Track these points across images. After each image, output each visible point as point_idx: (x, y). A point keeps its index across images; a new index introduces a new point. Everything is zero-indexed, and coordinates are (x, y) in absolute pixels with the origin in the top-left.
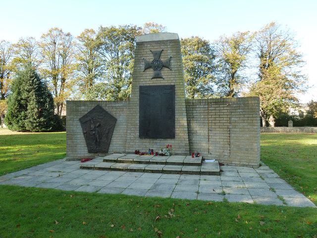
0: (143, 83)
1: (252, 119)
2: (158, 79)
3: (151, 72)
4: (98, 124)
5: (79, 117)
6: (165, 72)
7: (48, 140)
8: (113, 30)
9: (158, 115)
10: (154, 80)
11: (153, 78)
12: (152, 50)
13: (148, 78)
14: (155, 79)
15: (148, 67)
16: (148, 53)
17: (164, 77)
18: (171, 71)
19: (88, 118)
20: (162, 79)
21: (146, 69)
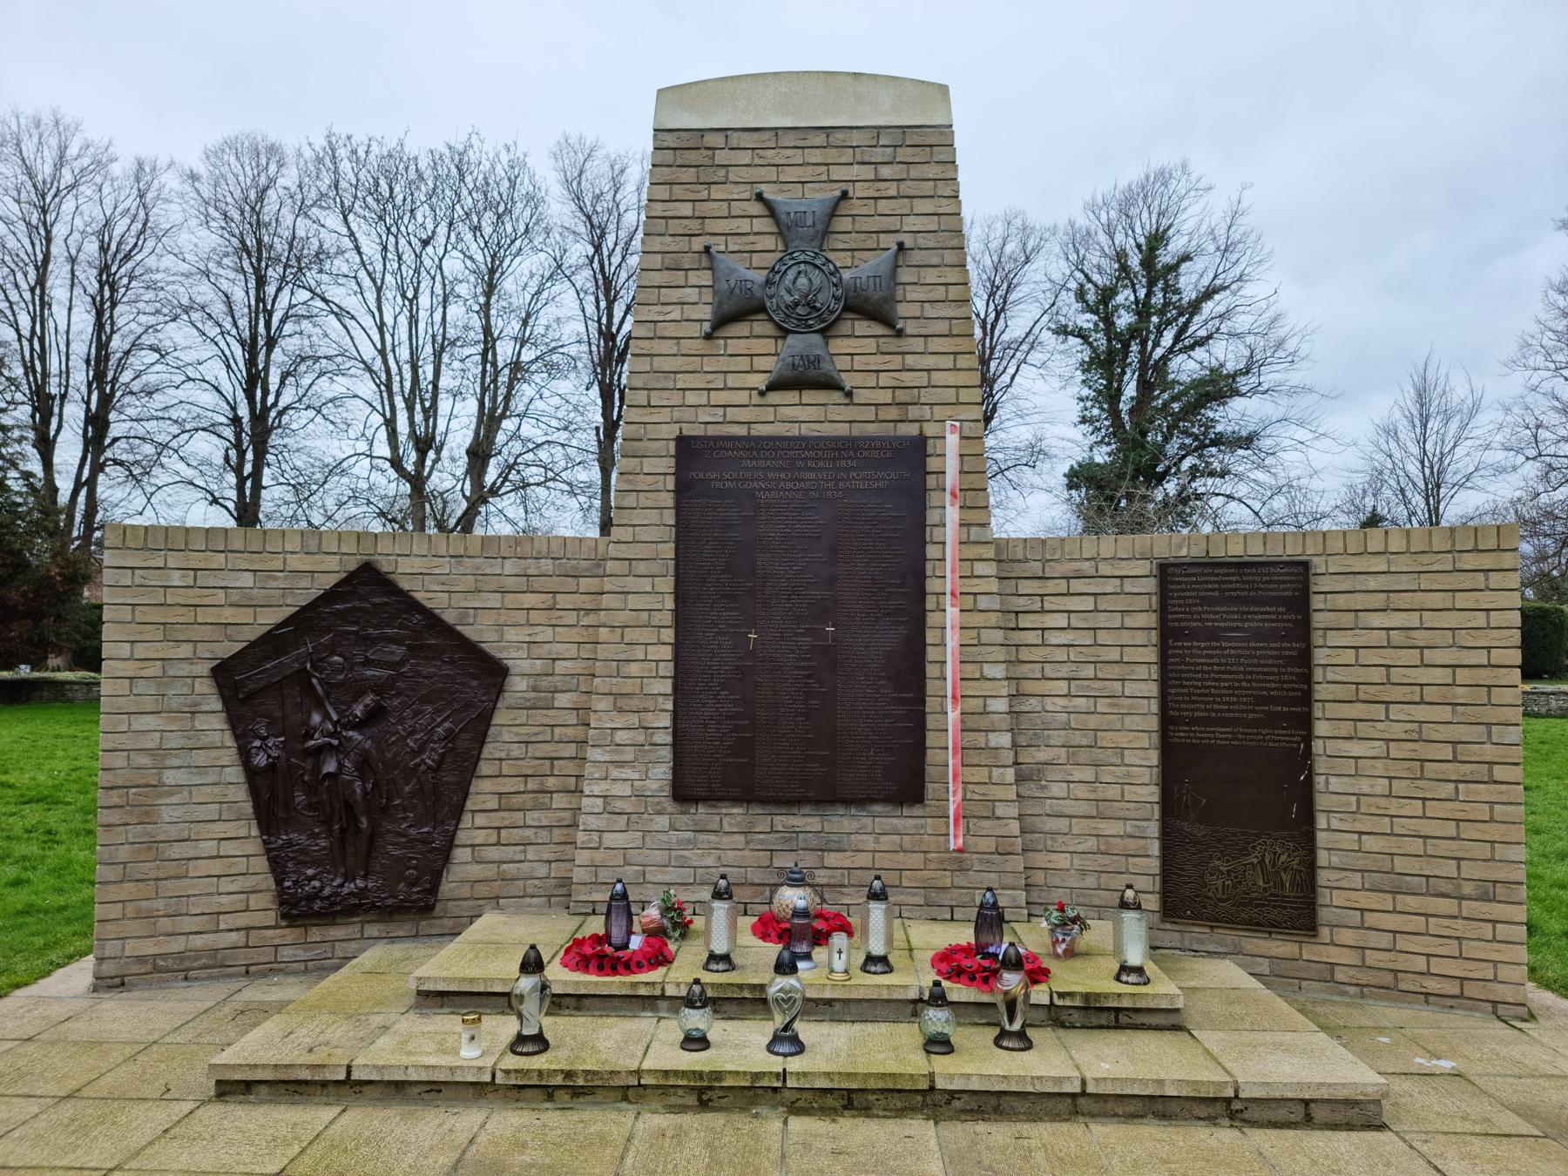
0: (704, 417)
1: (1484, 676)
2: (809, 396)
3: (757, 351)
4: (369, 699)
5: (518, 685)
6: (855, 349)
7: (157, 1147)
8: (393, 167)
9: (801, 634)
10: (774, 397)
11: (773, 387)
12: (769, 193)
13: (734, 390)
14: (791, 396)
15: (735, 311)
16: (737, 208)
17: (848, 381)
18: (893, 344)
19: (289, 661)
20: (837, 396)
21: (722, 321)
